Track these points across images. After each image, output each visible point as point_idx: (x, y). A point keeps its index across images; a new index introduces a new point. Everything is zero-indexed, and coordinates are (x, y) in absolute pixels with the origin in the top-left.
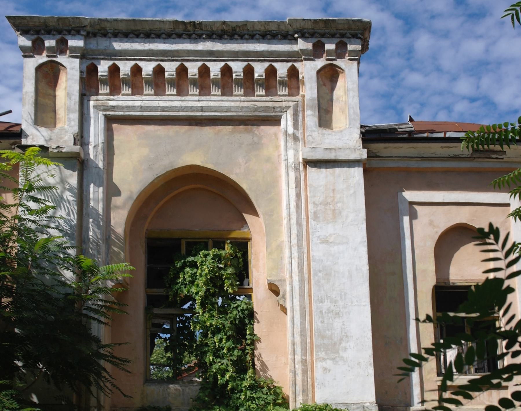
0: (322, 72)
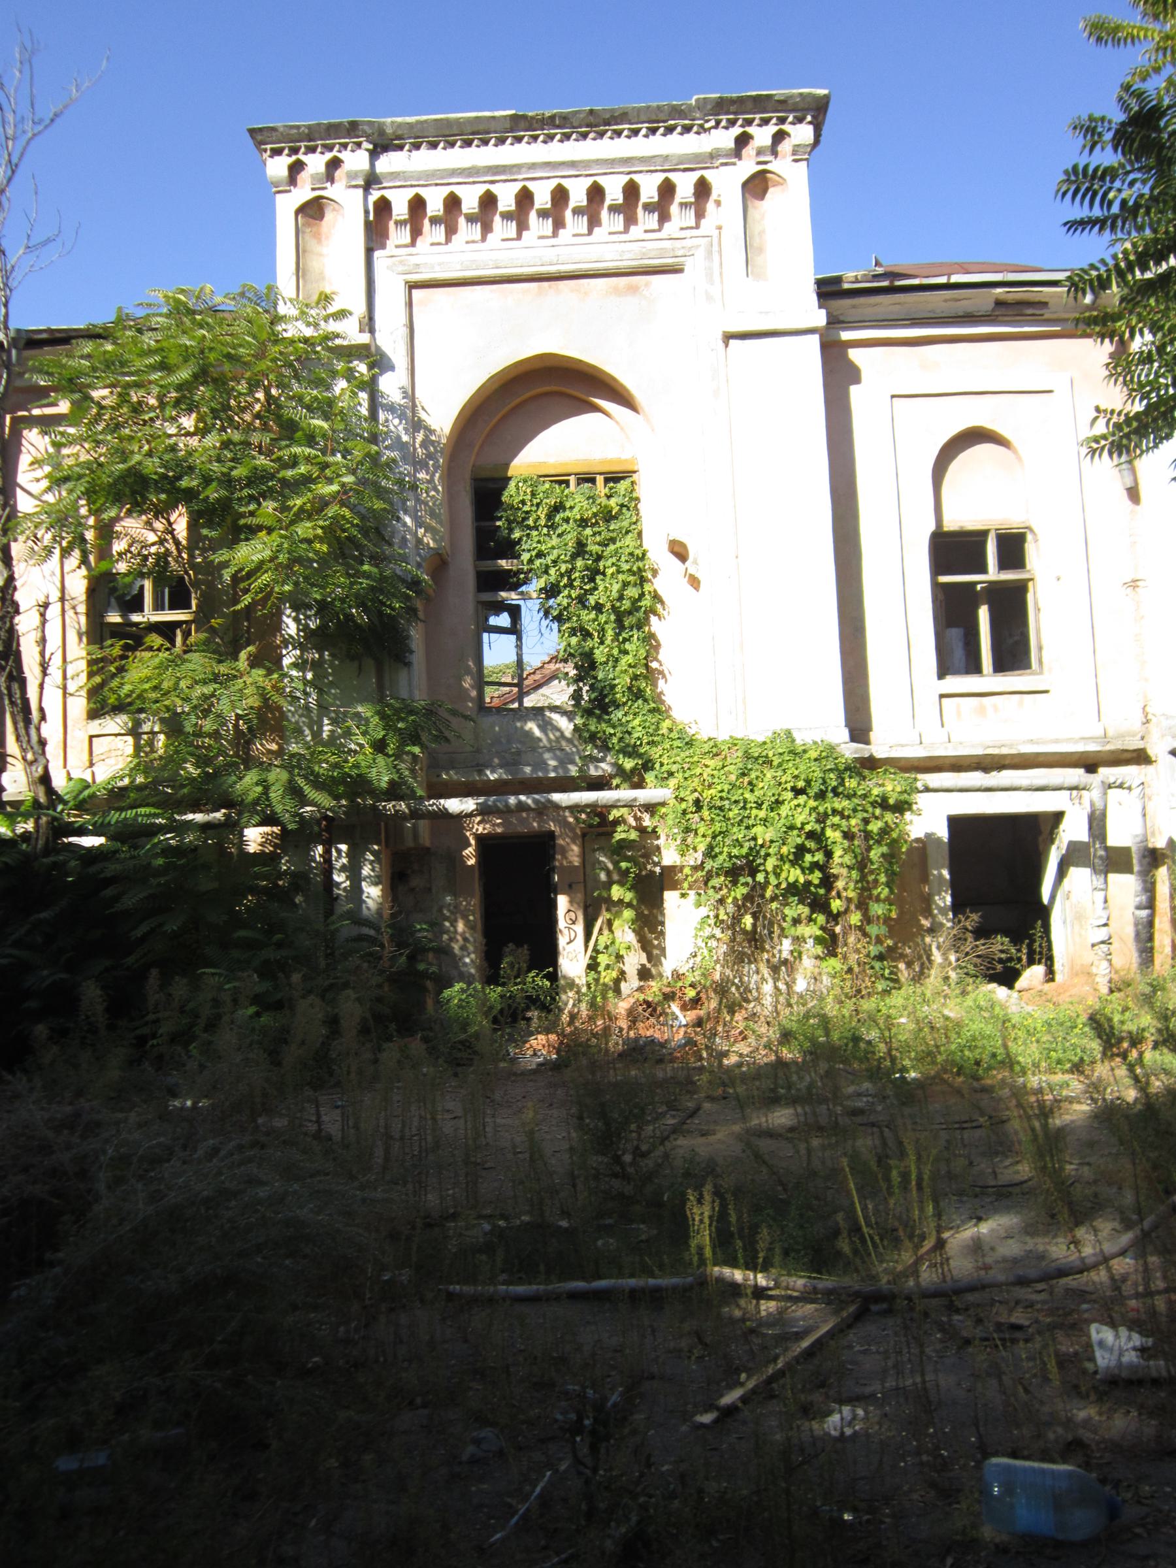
0: (750, 185)
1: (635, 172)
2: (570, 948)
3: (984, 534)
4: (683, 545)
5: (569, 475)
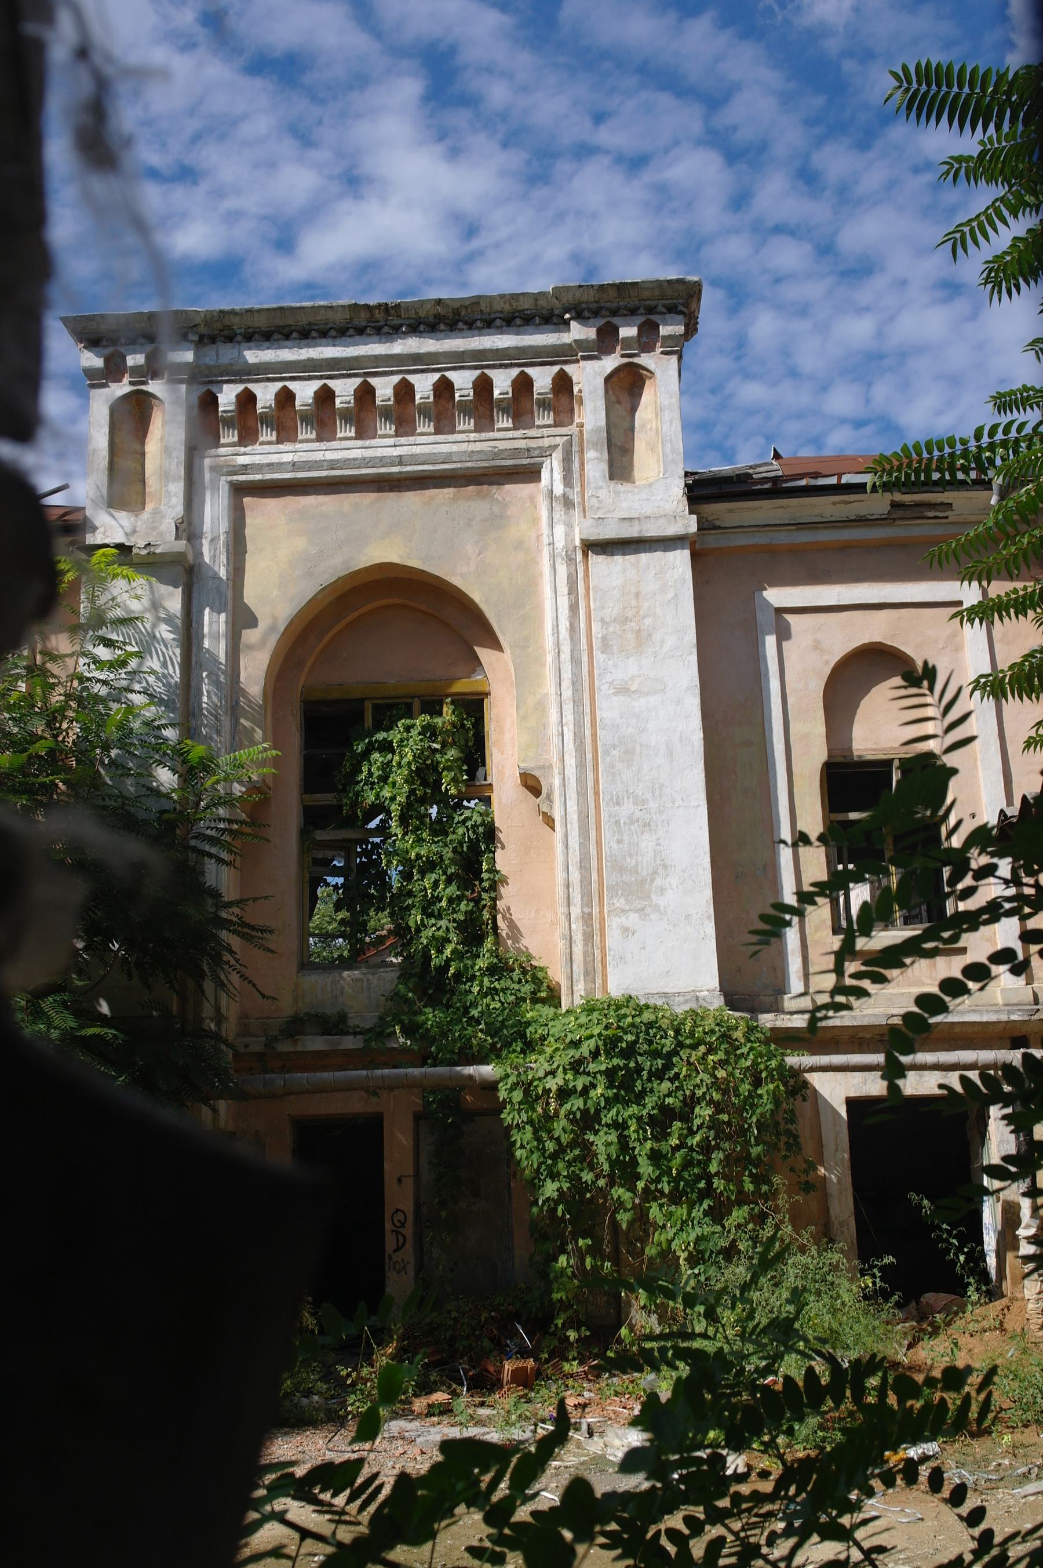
0: (614, 379)
1: (488, 367)
2: (396, 1257)
3: (889, 762)
5: (413, 697)
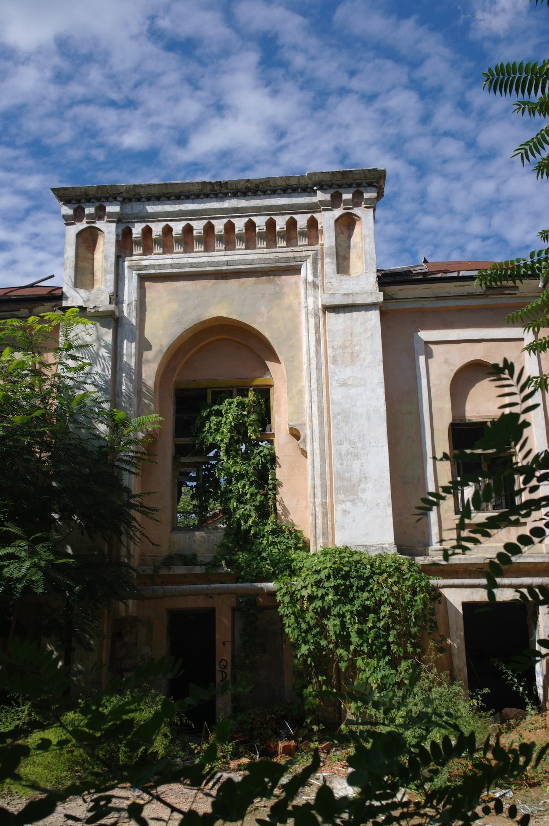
0: (340, 221)
1: (191, 220)
4: (297, 431)
5: (233, 387)
